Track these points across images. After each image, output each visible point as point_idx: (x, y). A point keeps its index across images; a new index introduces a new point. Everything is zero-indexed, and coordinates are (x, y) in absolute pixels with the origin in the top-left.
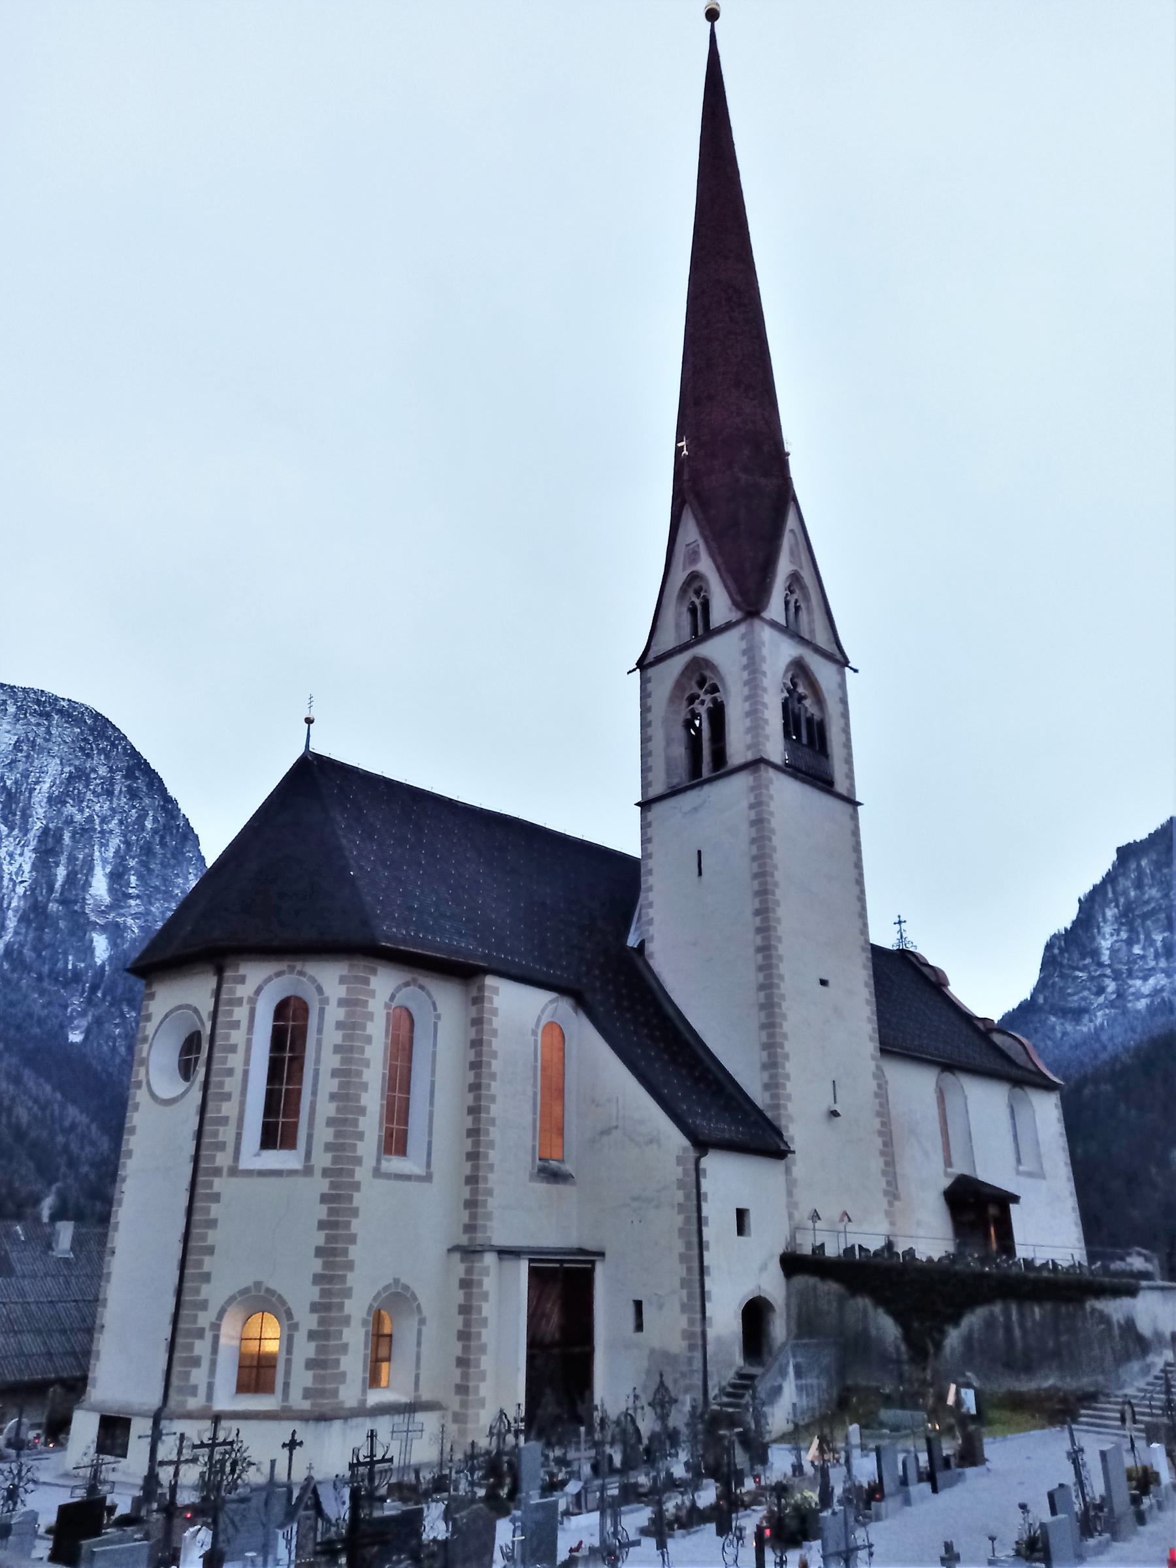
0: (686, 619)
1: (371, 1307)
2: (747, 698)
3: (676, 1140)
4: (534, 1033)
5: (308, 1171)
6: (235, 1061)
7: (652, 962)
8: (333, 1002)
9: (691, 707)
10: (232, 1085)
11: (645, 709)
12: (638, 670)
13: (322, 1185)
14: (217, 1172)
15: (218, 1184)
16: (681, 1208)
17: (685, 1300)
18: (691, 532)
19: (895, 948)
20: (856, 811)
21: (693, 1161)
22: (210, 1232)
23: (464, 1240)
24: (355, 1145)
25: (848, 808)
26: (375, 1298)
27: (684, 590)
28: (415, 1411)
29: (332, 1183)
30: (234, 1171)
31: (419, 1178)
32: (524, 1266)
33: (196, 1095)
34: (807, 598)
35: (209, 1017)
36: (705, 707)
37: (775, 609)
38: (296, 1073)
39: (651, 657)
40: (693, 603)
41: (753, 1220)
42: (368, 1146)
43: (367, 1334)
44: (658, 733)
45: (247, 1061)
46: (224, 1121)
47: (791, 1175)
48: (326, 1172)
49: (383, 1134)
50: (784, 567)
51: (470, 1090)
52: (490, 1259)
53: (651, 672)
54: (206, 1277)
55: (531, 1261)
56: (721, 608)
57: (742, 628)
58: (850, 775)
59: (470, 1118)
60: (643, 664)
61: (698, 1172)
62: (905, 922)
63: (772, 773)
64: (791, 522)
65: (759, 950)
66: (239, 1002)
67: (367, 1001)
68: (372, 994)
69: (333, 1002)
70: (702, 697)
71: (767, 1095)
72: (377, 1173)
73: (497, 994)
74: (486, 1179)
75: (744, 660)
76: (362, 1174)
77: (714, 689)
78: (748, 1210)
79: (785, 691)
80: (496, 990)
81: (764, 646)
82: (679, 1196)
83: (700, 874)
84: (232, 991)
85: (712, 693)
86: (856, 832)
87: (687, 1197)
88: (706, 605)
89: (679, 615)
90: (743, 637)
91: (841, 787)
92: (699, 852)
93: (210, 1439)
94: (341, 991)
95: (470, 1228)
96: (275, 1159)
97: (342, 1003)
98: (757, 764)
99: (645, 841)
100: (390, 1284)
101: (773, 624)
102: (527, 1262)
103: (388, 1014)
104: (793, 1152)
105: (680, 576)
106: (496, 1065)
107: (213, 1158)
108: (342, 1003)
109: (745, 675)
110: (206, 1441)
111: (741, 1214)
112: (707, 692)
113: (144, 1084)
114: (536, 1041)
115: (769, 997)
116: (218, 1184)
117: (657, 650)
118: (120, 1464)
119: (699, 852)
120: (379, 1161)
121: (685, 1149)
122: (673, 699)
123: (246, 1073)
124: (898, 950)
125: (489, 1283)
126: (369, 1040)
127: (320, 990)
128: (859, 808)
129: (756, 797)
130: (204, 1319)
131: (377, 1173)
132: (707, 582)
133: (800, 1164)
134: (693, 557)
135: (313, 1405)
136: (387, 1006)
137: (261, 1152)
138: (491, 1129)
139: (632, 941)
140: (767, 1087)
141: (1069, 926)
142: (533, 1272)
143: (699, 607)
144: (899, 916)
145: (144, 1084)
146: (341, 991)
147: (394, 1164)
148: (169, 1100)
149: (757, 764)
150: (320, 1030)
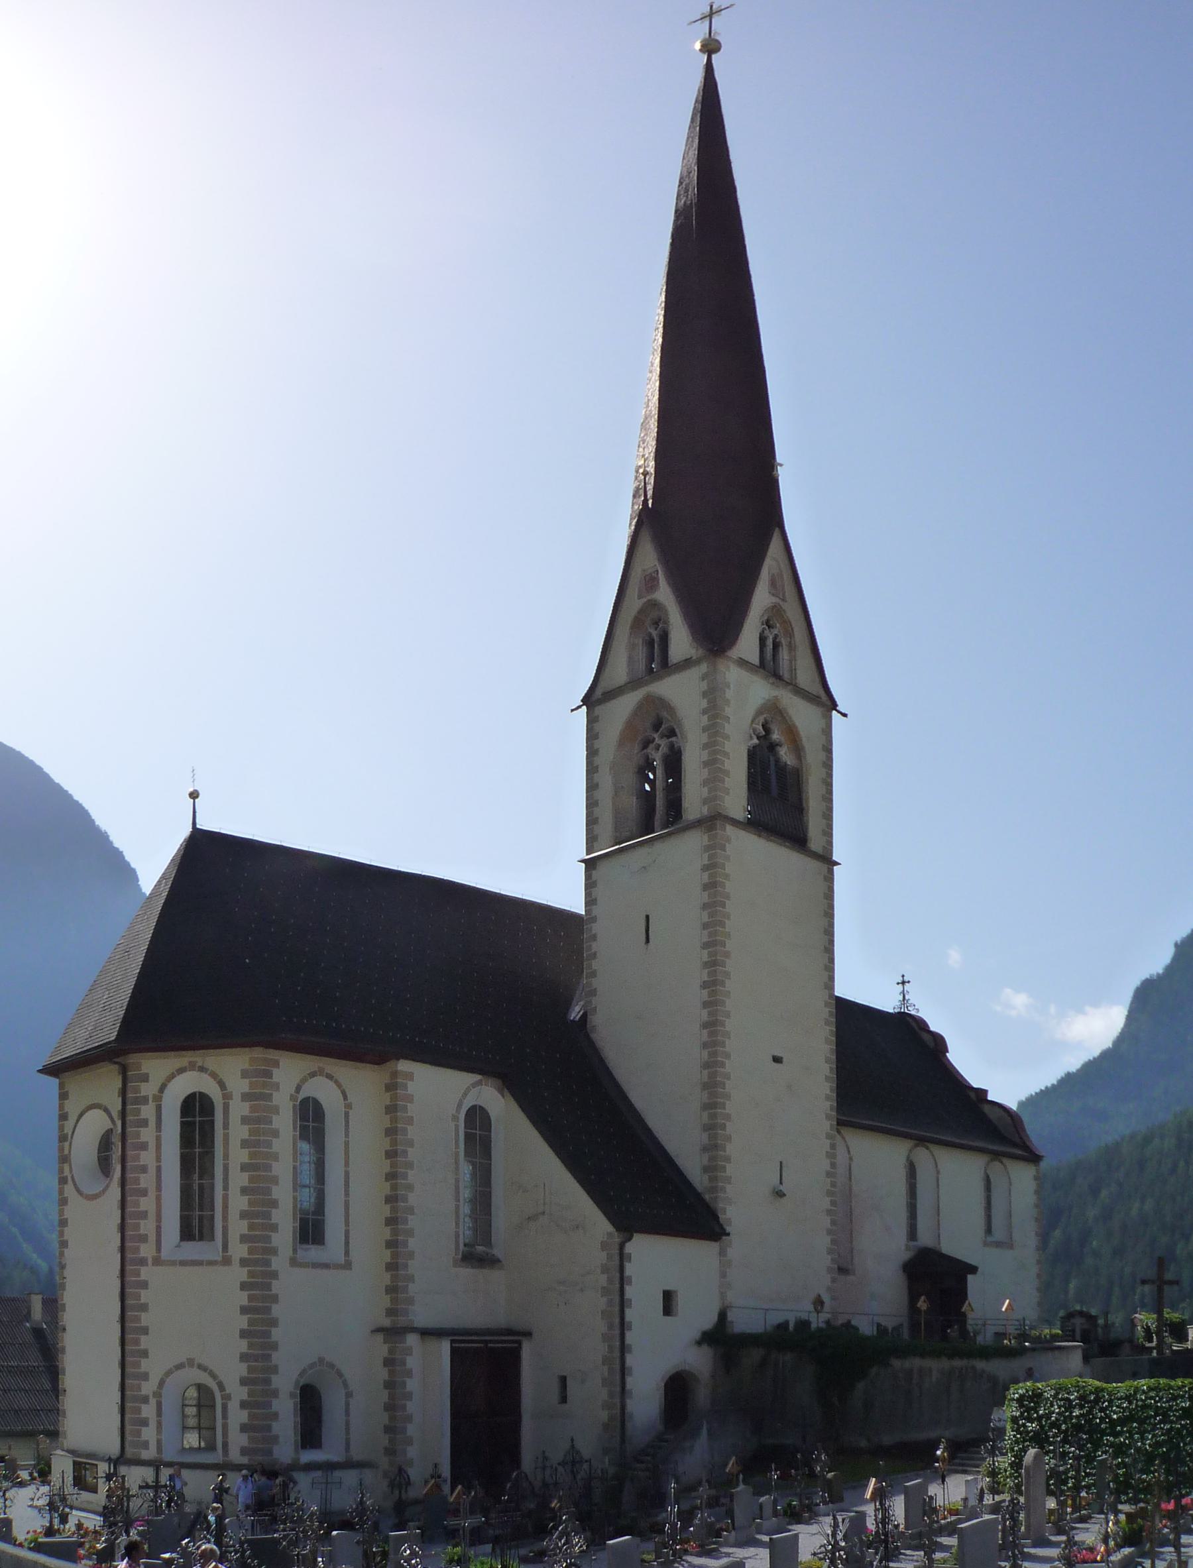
0: (641, 653)
1: (297, 1382)
2: (705, 746)
3: (601, 1225)
4: (455, 1118)
5: (227, 1261)
6: (147, 1158)
7: (593, 1036)
8: (237, 1097)
9: (645, 751)
10: (146, 1181)
11: (592, 752)
12: (584, 708)
13: (242, 1274)
14: (143, 1262)
15: (145, 1273)
16: (605, 1291)
17: (606, 1374)
18: (649, 558)
19: (897, 1010)
20: (831, 872)
21: (617, 1247)
22: (143, 1315)
23: (387, 1322)
24: (270, 1236)
25: (825, 867)
26: (301, 1375)
27: (637, 623)
28: (335, 1469)
29: (249, 1272)
30: (157, 1261)
31: (338, 1266)
32: (445, 1347)
33: (115, 1191)
34: (790, 634)
35: (119, 1116)
36: (660, 753)
37: (747, 644)
38: (207, 1171)
39: (598, 693)
40: (650, 635)
41: (681, 1302)
42: (284, 1236)
43: (295, 1404)
44: (606, 780)
45: (158, 1159)
46: (144, 1215)
47: (725, 1255)
48: (244, 1262)
49: (298, 1225)
50: (761, 599)
51: (387, 1180)
52: (412, 1340)
53: (598, 710)
54: (145, 1354)
55: (452, 1342)
56: (681, 643)
57: (704, 667)
58: (828, 832)
59: (388, 1207)
60: (589, 700)
61: (623, 1257)
62: (909, 982)
63: (730, 829)
64: (775, 546)
65: (705, 1025)
66: (145, 1100)
67: (271, 1094)
68: (277, 1087)
69: (237, 1097)
70: (657, 741)
71: (706, 1177)
72: (294, 1262)
73: (412, 1079)
74: (406, 1266)
75: (704, 704)
76: (279, 1263)
77: (672, 733)
78: (675, 1292)
79: (755, 737)
80: (410, 1076)
81: (729, 687)
82: (603, 1280)
83: (648, 941)
84: (137, 1090)
85: (668, 737)
86: (829, 895)
87: (610, 1281)
88: (665, 638)
89: (632, 647)
90: (704, 677)
91: (815, 844)
92: (647, 917)
93: (153, 1482)
94: (243, 1086)
95: (391, 1312)
96: (193, 1250)
97: (246, 1097)
98: (712, 821)
99: (590, 901)
100: (315, 1362)
101: (743, 663)
102: (449, 1342)
103: (294, 1106)
104: (728, 1234)
105: (634, 604)
106: (413, 1154)
107: (137, 1249)
108: (246, 1097)
109: (705, 720)
110: (151, 1484)
111: (668, 1298)
112: (662, 736)
113: (69, 1178)
114: (457, 1127)
115: (713, 1075)
116: (145, 1273)
117: (606, 685)
118: (81, 1496)
119: (647, 917)
120: (295, 1251)
121: (610, 1235)
122: (623, 741)
123: (159, 1169)
124: (899, 1013)
125: (412, 1362)
126: (276, 1133)
127: (222, 1085)
128: (835, 868)
129: (710, 857)
130: (148, 1388)
131: (294, 1262)
132: (666, 613)
133: (737, 1246)
134: (650, 583)
135: (249, 1460)
136: (293, 1098)
137: (182, 1243)
138: (410, 1217)
139: (575, 1013)
140: (706, 1169)
141: (1161, 971)
142: (454, 1351)
143: (656, 639)
144: (903, 976)
145: (69, 1178)
146: (243, 1086)
147: (313, 1253)
148: (93, 1195)
149: (712, 821)
150: (226, 1126)
